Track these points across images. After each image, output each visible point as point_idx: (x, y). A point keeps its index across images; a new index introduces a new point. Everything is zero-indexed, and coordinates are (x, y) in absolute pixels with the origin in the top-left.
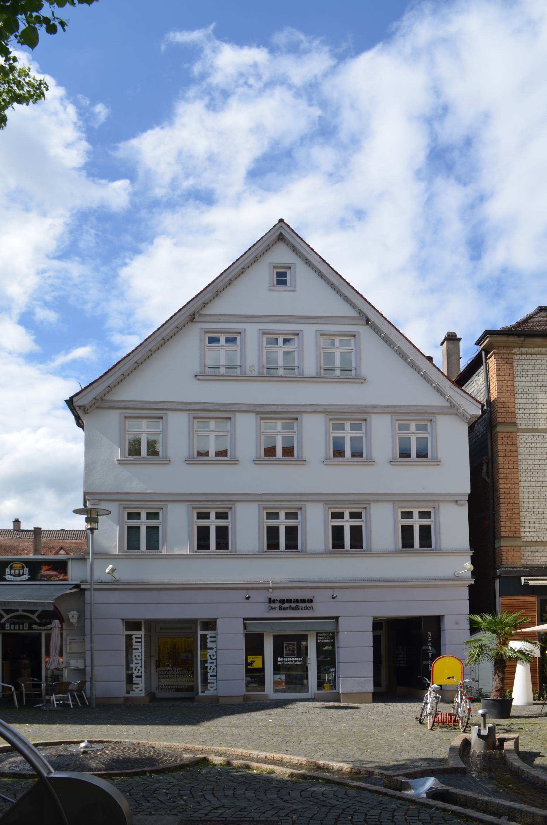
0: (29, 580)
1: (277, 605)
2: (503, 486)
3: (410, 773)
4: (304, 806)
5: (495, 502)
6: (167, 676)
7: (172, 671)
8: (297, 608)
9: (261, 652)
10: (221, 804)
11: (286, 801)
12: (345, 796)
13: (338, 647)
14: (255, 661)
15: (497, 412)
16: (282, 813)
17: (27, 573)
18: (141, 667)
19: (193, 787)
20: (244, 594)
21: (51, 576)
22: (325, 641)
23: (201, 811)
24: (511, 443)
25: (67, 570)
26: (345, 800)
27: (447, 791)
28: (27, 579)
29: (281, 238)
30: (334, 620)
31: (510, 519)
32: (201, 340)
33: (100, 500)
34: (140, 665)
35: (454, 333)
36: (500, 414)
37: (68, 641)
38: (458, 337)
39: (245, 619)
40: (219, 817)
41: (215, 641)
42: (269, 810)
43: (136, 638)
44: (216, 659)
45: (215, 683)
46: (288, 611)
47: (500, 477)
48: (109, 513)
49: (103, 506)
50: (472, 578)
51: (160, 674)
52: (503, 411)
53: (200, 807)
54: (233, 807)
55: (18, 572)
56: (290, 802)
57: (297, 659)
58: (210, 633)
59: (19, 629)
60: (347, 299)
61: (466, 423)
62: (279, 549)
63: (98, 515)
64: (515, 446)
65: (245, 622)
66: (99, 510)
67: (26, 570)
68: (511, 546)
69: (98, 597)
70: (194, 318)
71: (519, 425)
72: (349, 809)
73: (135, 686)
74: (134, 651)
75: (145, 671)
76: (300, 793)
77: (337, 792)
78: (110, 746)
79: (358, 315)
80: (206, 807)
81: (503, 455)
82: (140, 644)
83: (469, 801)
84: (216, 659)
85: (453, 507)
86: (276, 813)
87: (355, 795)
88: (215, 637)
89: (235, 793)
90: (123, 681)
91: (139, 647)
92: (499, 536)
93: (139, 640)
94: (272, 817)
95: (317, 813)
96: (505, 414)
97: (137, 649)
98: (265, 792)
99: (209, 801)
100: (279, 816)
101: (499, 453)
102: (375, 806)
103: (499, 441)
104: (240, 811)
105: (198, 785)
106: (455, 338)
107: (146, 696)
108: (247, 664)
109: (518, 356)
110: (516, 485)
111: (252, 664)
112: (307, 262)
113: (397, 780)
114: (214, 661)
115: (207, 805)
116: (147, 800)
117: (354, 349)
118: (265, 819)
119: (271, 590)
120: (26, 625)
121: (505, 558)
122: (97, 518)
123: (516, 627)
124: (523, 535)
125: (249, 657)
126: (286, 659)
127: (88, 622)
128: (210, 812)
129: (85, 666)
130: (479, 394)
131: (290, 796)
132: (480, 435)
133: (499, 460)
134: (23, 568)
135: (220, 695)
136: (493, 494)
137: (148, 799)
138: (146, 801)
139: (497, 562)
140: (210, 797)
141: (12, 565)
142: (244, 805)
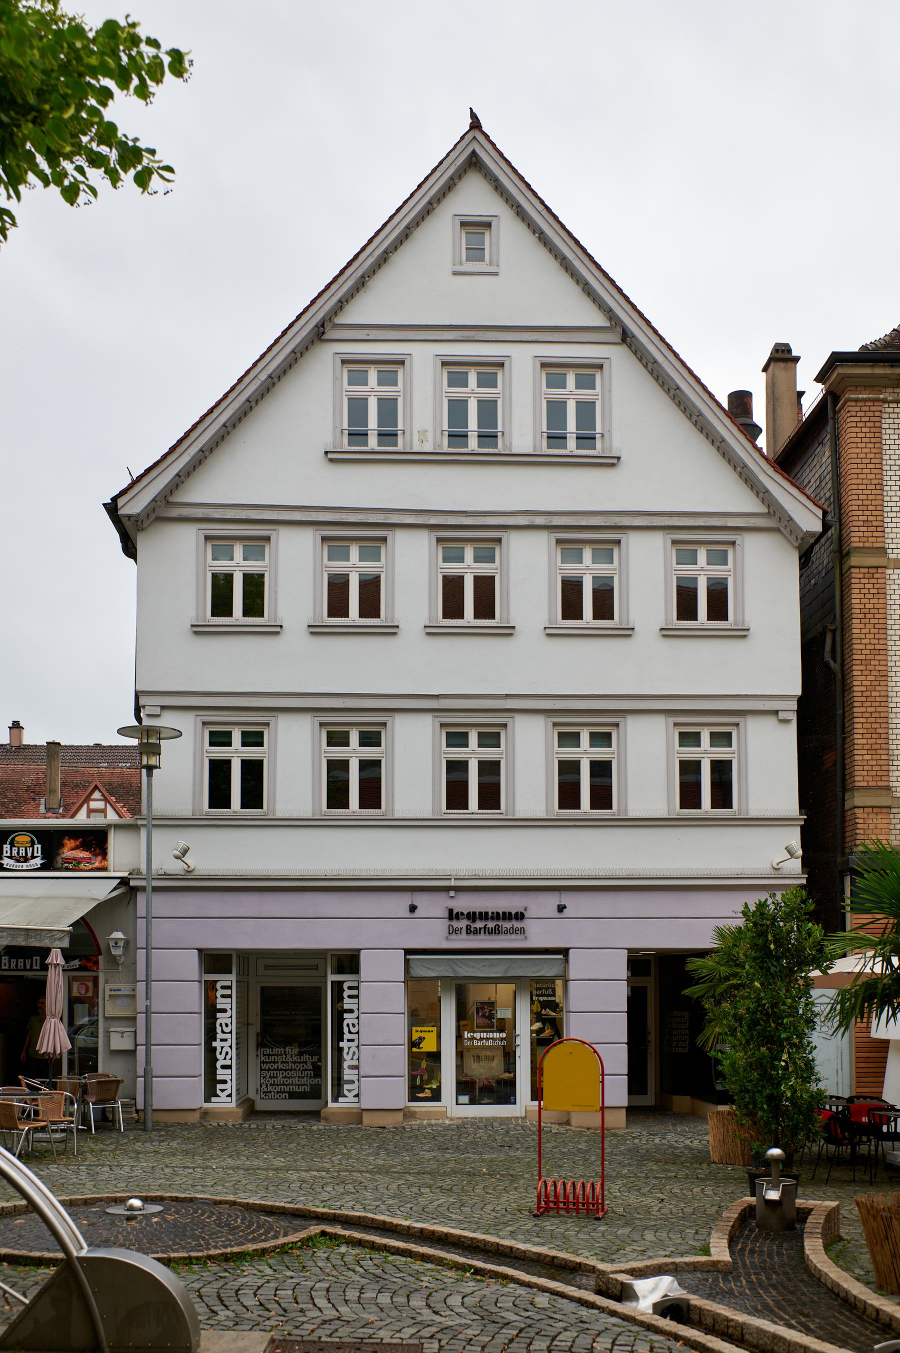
0: (43, 868)
1: (463, 924)
2: (860, 681)
3: (638, 1268)
4: (463, 1321)
5: (846, 714)
6: (275, 1066)
7: (284, 1056)
8: (497, 931)
9: (436, 1022)
10: (337, 1314)
11: (436, 1313)
12: (530, 1307)
13: (567, 1012)
14: (424, 1038)
15: (851, 524)
16: (426, 1332)
17: (39, 854)
18: (231, 1047)
19: (298, 1284)
20: (406, 900)
21: (79, 861)
22: (545, 998)
23: (306, 1326)
24: (875, 591)
25: (107, 849)
26: (527, 1314)
27: (687, 1301)
28: (39, 866)
29: (474, 163)
30: (561, 957)
31: (871, 750)
32: (335, 378)
33: (163, 708)
34: (228, 1043)
35: (787, 345)
36: (856, 529)
37: (108, 993)
38: (794, 354)
39: (408, 952)
40: (330, 1336)
41: (357, 997)
42: (408, 1327)
43: (223, 987)
44: (358, 1033)
45: (356, 1082)
46: (482, 936)
47: (854, 662)
48: (180, 734)
49: (168, 721)
50: (803, 873)
51: (263, 1062)
52: (861, 524)
53: (304, 1319)
54: (354, 1321)
55: (24, 852)
56: (442, 1313)
57: (497, 1035)
58: (347, 979)
59: (25, 969)
60: (588, 291)
61: (796, 548)
62: (467, 809)
63: (160, 739)
64: (883, 596)
65: (408, 957)
66: (162, 729)
67: (38, 846)
68: (872, 807)
69: (162, 904)
70: (323, 333)
71: (889, 551)
72: (530, 1329)
73: (219, 1086)
74: (219, 1015)
75: (237, 1055)
76: (463, 1298)
77: (520, 1299)
78: (174, 1207)
79: (608, 324)
80: (313, 1318)
81: (861, 616)
82: (229, 1000)
83: (717, 1322)
84: (358, 1033)
85: (770, 723)
86: (418, 1332)
87: (547, 1305)
88: (357, 988)
89: (362, 1296)
90: (200, 1075)
91: (228, 1007)
92: (851, 786)
93: (228, 992)
94: (410, 1338)
95: (478, 1335)
96: (865, 529)
97: (225, 1011)
98: (408, 1296)
99: (320, 1309)
100: (422, 1338)
101: (853, 611)
102: (572, 1325)
103: (853, 586)
104: (363, 1327)
105: (306, 1281)
106: (788, 356)
107: (237, 1106)
108: (413, 1044)
109: (891, 405)
110: (883, 678)
111: (420, 1043)
112: (520, 213)
113: (616, 1280)
114: (355, 1036)
115: (315, 1316)
116: (226, 1306)
117: (600, 394)
118: (400, 1341)
119: (452, 893)
120: (36, 960)
121: (862, 832)
122: (159, 745)
123: (71, 1203)
124: (895, 784)
125: (414, 1029)
126: (477, 1035)
127: (141, 954)
128: (318, 1328)
129: (136, 1045)
130: (823, 484)
131: (446, 1303)
132: (824, 570)
133: (853, 626)
134: (33, 844)
135: (363, 1107)
136: (843, 697)
137: (227, 1303)
138: (223, 1308)
139: (848, 839)
140: (321, 1302)
141: (13, 839)
142: (372, 1318)
